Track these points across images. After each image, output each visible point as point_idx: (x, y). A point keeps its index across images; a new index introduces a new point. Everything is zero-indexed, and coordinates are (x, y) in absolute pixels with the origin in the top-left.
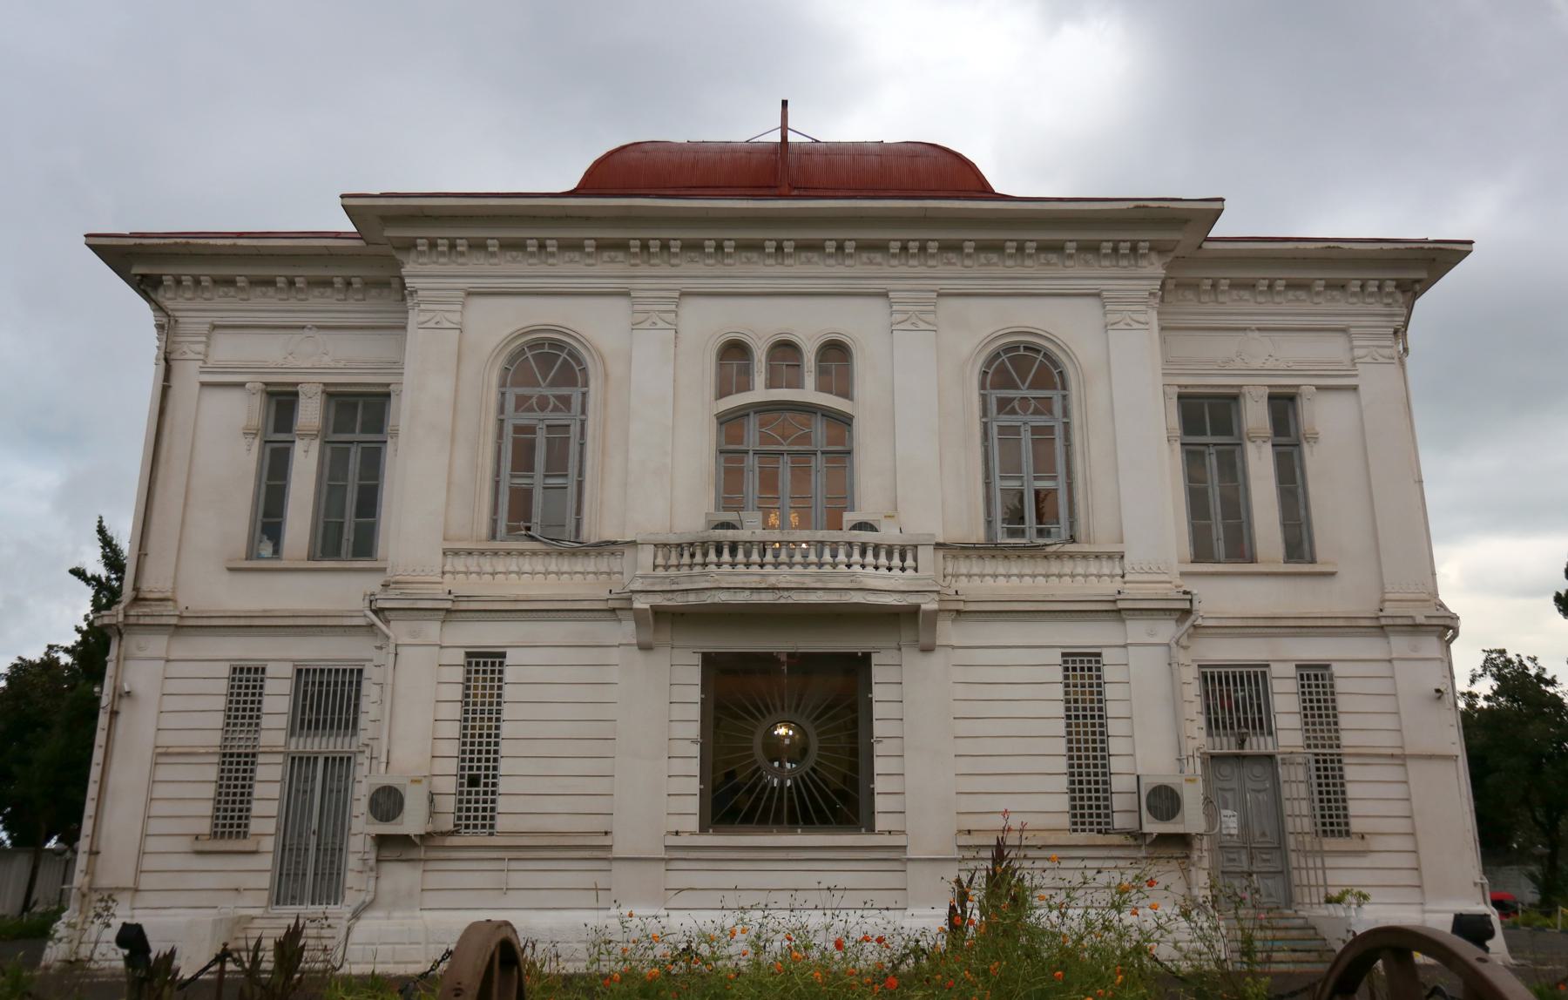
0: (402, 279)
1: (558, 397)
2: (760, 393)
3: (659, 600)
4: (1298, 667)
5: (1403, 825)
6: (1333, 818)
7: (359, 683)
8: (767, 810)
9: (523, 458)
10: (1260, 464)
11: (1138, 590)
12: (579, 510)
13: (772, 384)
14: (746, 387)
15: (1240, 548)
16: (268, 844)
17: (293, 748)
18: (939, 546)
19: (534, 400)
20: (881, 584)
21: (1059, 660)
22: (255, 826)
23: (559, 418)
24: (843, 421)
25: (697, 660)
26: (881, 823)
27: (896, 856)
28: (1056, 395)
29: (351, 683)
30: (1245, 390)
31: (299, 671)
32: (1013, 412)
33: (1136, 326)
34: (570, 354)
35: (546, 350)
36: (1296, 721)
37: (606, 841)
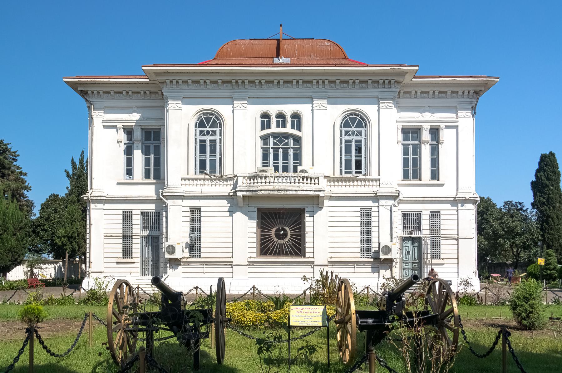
0: (162, 93)
2: (274, 129)
3: (245, 193)
4: (430, 212)
6: (436, 254)
7: (159, 216)
8: (276, 251)
9: (203, 150)
10: (426, 151)
11: (383, 190)
13: (278, 126)
14: (269, 127)
15: (417, 175)
16: (139, 260)
18: (326, 177)
20: (308, 189)
21: (360, 210)
22: (134, 255)
24: (298, 140)
25: (255, 210)
26: (307, 255)
31: (142, 213)
33: (388, 107)
34: (216, 117)
36: (428, 227)
37: (231, 260)
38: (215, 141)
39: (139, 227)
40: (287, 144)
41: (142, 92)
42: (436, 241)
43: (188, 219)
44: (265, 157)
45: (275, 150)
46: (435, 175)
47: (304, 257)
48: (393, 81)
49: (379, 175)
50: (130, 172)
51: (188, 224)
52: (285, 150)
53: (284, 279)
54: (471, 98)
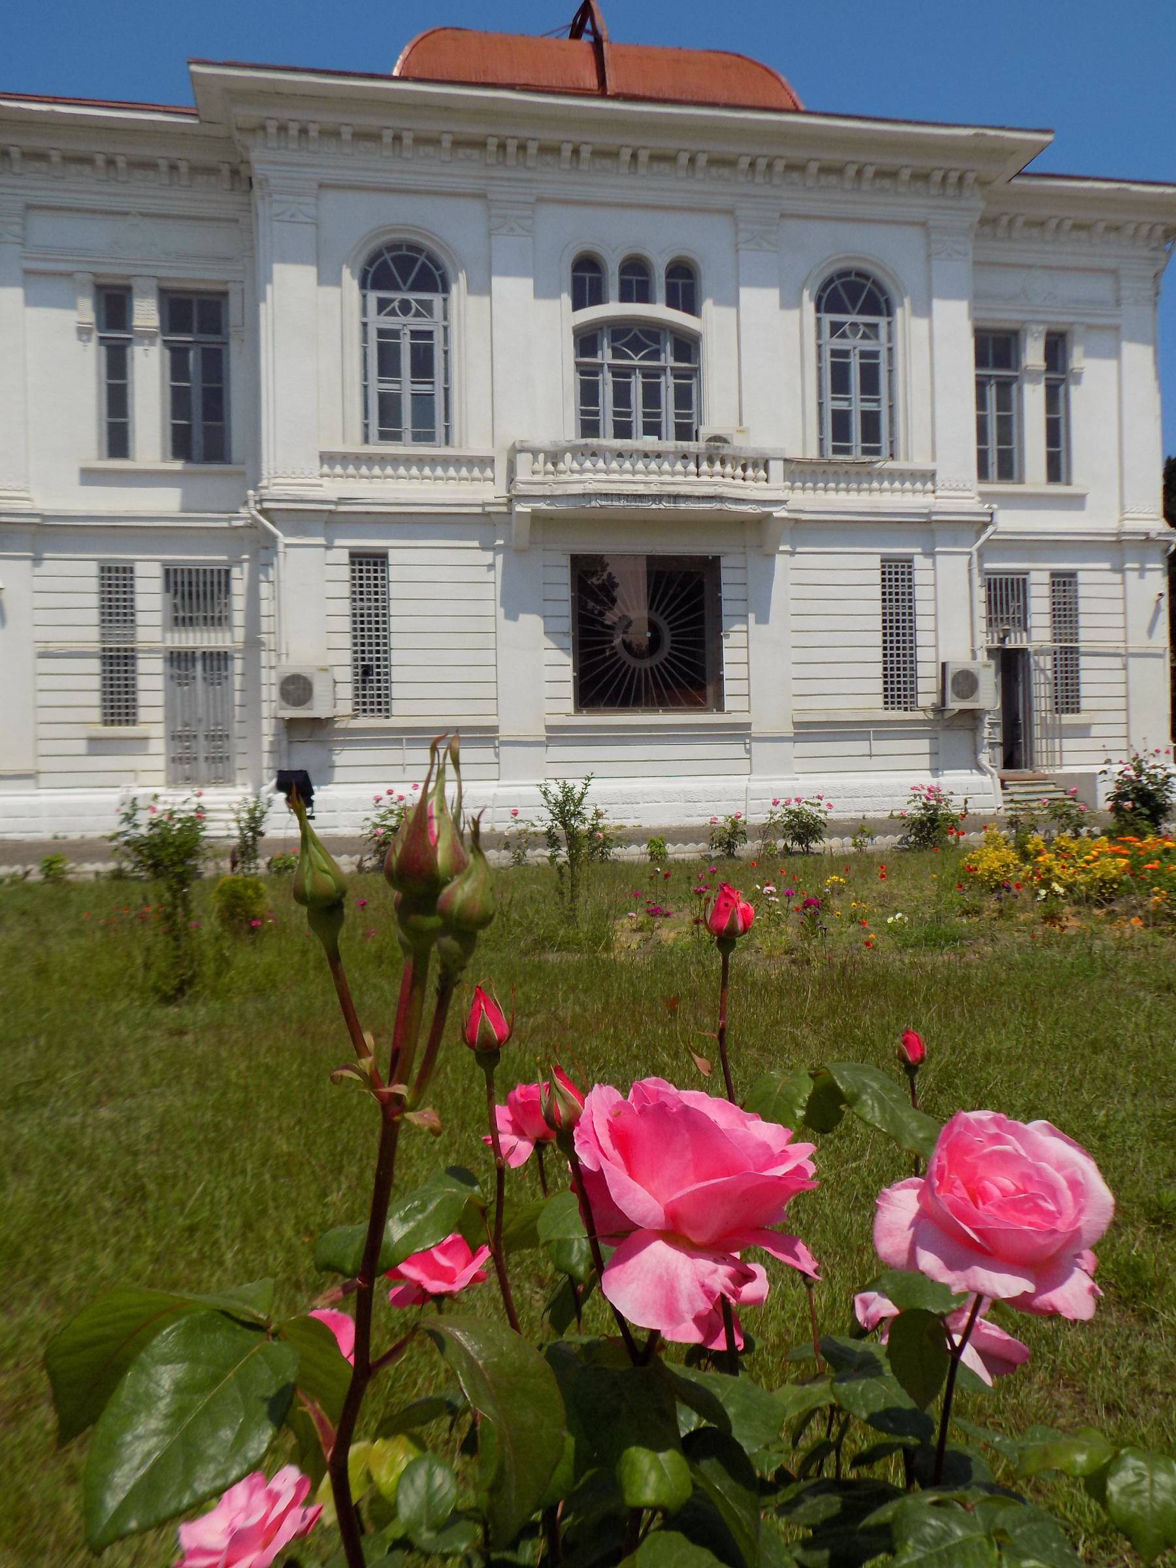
1: (867, 325)
2: (613, 308)
5: (1121, 703)
12: (447, 417)
14: (598, 298)
16: (158, 731)
17: (169, 644)
19: (396, 304)
22: (143, 715)
23: (422, 324)
26: (729, 703)
27: (739, 732)
28: (436, 299)
29: (219, 583)
30: (230, 286)
31: (167, 572)
32: (844, 336)
34: (875, 283)
35: (404, 252)
36: (1046, 620)
38: (429, 335)
39: (157, 618)
40: (655, 355)
41: (163, 163)
42: (1067, 660)
43: (345, 590)
44: (589, 394)
45: (617, 372)
46: (1056, 469)
47: (720, 708)
48: (970, 177)
49: (934, 459)
50: (118, 440)
51: (345, 607)
52: (648, 373)
53: (659, 785)
54: (1154, 249)
